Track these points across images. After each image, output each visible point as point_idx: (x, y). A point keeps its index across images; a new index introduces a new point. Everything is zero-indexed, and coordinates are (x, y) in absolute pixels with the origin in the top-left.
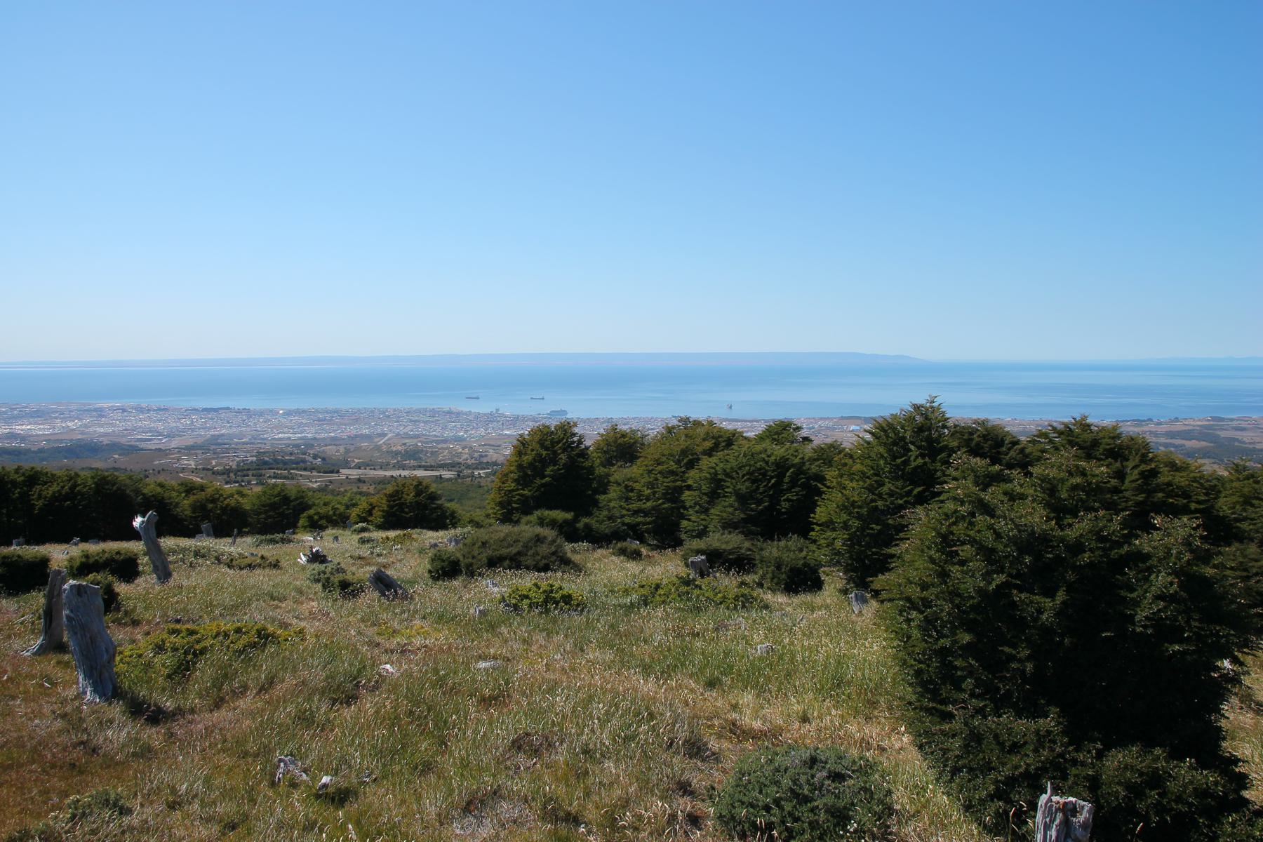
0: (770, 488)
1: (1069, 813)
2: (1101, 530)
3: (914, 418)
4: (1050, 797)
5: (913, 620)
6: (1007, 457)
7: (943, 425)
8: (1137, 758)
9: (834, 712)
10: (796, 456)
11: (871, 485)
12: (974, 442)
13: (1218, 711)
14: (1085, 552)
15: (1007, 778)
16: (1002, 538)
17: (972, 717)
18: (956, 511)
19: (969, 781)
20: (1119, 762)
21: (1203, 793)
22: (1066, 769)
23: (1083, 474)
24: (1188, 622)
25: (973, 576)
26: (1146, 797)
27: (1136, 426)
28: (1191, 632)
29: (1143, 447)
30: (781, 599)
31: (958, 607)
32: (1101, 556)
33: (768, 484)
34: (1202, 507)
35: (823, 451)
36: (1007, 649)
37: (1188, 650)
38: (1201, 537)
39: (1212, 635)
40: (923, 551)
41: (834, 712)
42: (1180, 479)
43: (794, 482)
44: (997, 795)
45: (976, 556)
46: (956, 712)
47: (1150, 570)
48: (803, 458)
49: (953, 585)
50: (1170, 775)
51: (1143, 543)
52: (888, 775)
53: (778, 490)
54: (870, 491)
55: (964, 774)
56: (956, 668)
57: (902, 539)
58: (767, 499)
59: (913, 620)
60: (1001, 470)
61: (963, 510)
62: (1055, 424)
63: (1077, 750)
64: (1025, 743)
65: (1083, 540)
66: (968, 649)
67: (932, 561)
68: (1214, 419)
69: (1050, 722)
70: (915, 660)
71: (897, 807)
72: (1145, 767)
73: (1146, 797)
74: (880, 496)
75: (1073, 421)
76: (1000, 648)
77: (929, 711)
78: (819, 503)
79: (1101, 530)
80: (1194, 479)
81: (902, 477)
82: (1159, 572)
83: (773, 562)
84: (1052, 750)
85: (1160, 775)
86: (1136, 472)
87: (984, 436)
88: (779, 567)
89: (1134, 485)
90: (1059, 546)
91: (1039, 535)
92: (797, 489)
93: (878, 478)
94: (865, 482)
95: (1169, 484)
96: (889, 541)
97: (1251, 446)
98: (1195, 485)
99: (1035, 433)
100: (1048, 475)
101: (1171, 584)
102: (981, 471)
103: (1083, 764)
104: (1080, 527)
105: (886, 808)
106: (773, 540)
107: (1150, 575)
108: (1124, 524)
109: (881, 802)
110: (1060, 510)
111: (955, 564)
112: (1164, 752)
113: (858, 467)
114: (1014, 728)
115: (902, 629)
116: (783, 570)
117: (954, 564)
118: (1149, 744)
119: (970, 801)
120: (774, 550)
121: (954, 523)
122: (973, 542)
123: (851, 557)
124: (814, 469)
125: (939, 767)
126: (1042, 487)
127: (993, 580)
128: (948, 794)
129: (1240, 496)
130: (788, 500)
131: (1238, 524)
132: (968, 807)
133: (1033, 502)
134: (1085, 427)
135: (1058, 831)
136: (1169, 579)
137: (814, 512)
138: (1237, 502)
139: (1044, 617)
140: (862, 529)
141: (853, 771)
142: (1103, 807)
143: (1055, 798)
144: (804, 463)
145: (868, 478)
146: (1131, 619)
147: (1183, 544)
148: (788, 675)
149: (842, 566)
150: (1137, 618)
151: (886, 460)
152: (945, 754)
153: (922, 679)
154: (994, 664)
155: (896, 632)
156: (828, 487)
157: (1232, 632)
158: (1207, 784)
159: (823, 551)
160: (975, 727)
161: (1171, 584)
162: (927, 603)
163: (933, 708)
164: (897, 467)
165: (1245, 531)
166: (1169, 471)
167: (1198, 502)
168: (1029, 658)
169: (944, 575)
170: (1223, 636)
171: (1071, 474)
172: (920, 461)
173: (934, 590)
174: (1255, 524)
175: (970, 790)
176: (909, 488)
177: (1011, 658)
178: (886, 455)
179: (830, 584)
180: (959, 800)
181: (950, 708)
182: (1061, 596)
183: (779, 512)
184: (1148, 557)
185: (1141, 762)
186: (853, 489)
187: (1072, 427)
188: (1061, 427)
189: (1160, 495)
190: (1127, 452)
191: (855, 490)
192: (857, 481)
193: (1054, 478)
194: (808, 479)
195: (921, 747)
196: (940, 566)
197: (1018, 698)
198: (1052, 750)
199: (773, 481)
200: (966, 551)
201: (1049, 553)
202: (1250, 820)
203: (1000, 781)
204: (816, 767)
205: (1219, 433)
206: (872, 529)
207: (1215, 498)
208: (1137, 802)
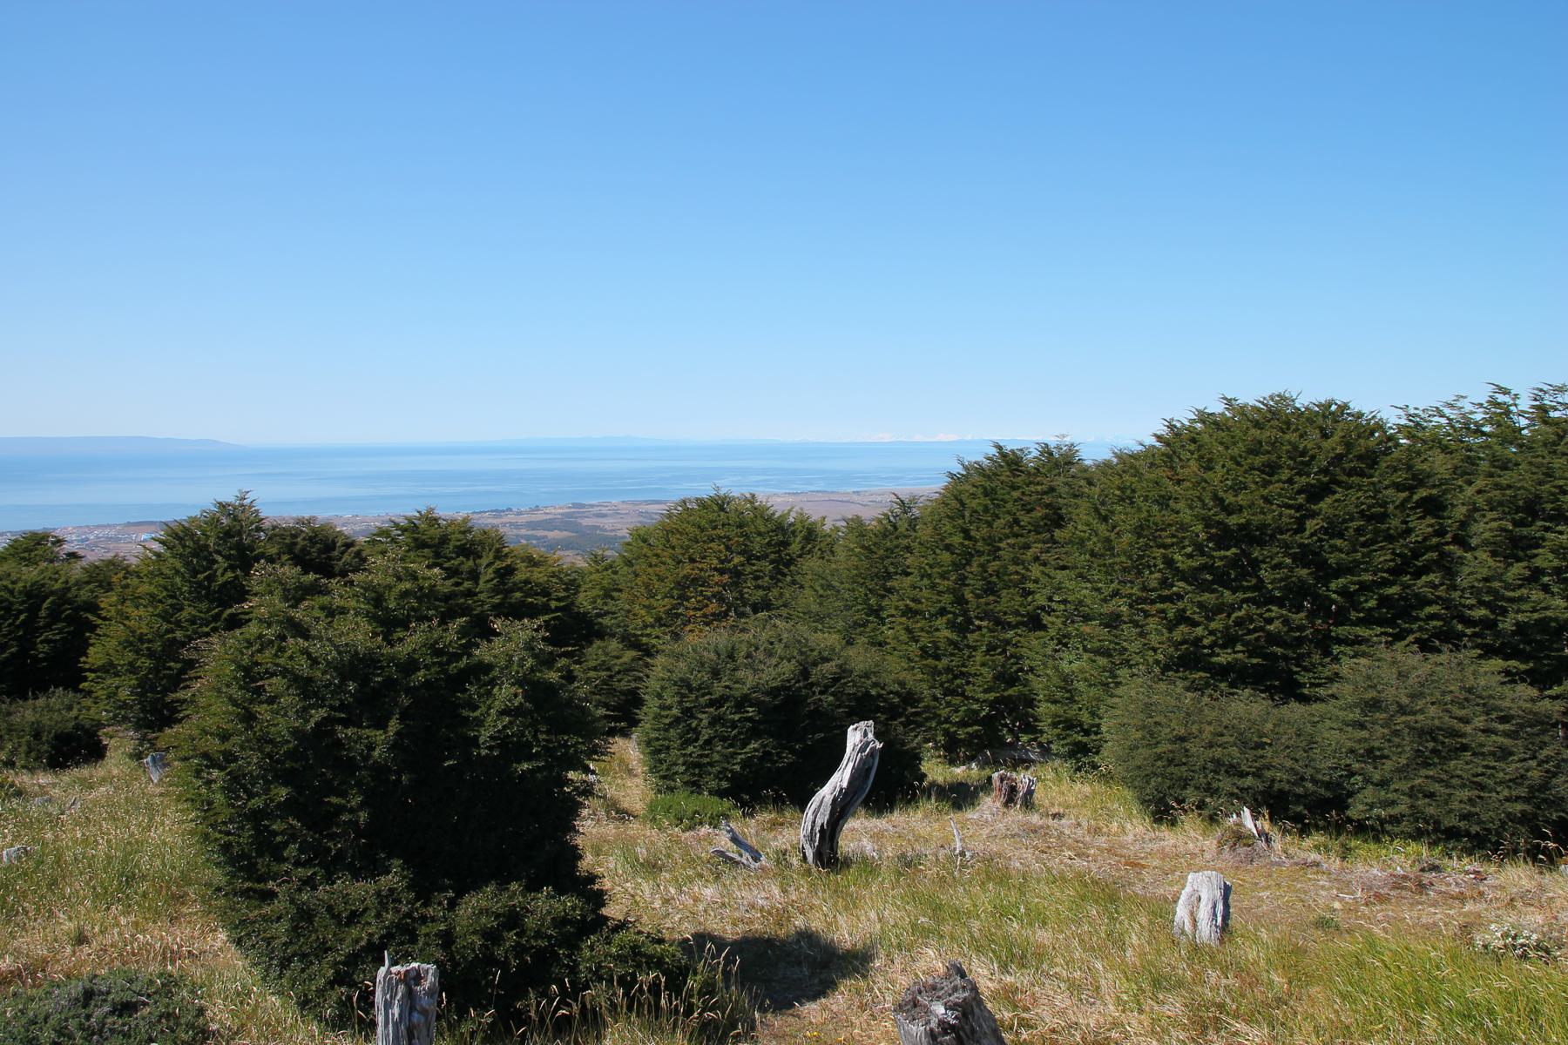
0: (18, 627)
1: (412, 982)
2: (436, 642)
3: (218, 521)
4: (389, 968)
5: (215, 781)
6: (341, 563)
7: (257, 527)
8: (492, 899)
9: (123, 921)
10: (56, 580)
11: (165, 611)
12: (298, 547)
13: (574, 830)
14: (419, 670)
15: (349, 956)
16: (319, 663)
17: (300, 890)
18: (260, 636)
19: (303, 970)
20: (473, 908)
21: (561, 922)
22: (415, 929)
23: (414, 576)
24: (535, 736)
25: (285, 715)
26: (504, 941)
27: (495, 517)
28: (538, 746)
29: (497, 541)
30: (44, 779)
31: (270, 756)
32: (437, 673)
33: (14, 622)
34: (562, 604)
35: (97, 571)
36: (335, 800)
37: (538, 767)
38: (544, 639)
39: (561, 746)
40: (219, 691)
41: (123, 921)
42: (539, 575)
43: (54, 615)
44: (340, 979)
45: (288, 689)
46: (277, 890)
47: (493, 682)
48: (67, 582)
49: (261, 730)
50: (528, 911)
51: (484, 652)
52: (201, 987)
53: (31, 628)
54: (164, 619)
55: (296, 964)
56: (275, 833)
57: (191, 679)
58: (14, 643)
59: (215, 781)
60: (316, 580)
61: (270, 633)
62: (397, 520)
63: (425, 905)
64: (366, 910)
65: (416, 656)
66: (288, 807)
67: (234, 702)
68: (575, 505)
69: (394, 878)
70: (220, 832)
71: (214, 1027)
72: (501, 907)
73: (504, 941)
74: (178, 623)
75: (418, 515)
76: (326, 800)
77: (246, 893)
78: (92, 641)
79: (436, 642)
80: (553, 575)
81: (207, 596)
82: (503, 683)
83: (27, 729)
84: (397, 911)
85: (518, 913)
86: (490, 570)
87: (311, 539)
88: (37, 735)
89: (489, 585)
90: (388, 666)
91: (365, 655)
92: (60, 625)
93: (175, 601)
94: (155, 608)
95: (527, 582)
96: (177, 682)
97: (613, 534)
98: (554, 580)
99: (375, 531)
100: (372, 581)
101: (516, 695)
102: (291, 583)
103: (433, 920)
104: (412, 641)
105: (197, 1034)
106: (26, 699)
107: (492, 688)
108: (463, 632)
109: (191, 1026)
110: (389, 624)
111: (263, 703)
112: (520, 886)
113: (145, 588)
114: (350, 894)
115: (200, 795)
116: (44, 739)
117: (261, 703)
118: (503, 884)
119: (306, 995)
120: (29, 712)
121: (259, 651)
122: (285, 672)
123: (143, 710)
124: (84, 595)
125: (265, 962)
126: (365, 598)
127: (311, 716)
128: (280, 993)
129: (601, 589)
130: (47, 641)
131: (600, 620)
132: (304, 1003)
133: (356, 615)
134: (432, 521)
135: (401, 1007)
136: (513, 690)
137: (86, 655)
138: (599, 596)
139: (376, 753)
140: (155, 670)
141: (149, 996)
142: (459, 964)
143: (394, 969)
144: (69, 589)
145: (160, 601)
146: (474, 742)
147: (525, 649)
148: (53, 883)
149: (130, 722)
150: (481, 740)
151: (183, 577)
152: (269, 944)
153: (232, 854)
154: (319, 818)
155: (192, 800)
156: (105, 619)
157: (580, 740)
158: (565, 911)
159: (101, 705)
160: (304, 903)
161: (516, 695)
162: (230, 757)
163: (249, 889)
164: (200, 584)
165: (608, 627)
166: (527, 567)
167: (558, 600)
168: (362, 806)
169: (249, 718)
170: (572, 746)
171: (400, 579)
172: (230, 574)
173: (235, 739)
174: (616, 618)
175: (304, 982)
176: (216, 610)
177: (340, 809)
178: (182, 570)
179: (117, 748)
180: (291, 998)
181: (271, 884)
182: (394, 725)
183: (35, 659)
184: (488, 668)
185: (497, 902)
186: (140, 617)
187: (416, 522)
188: (403, 523)
189: (518, 595)
190: (479, 548)
191: (142, 619)
192: (145, 606)
193: (379, 585)
194: (77, 609)
195: (239, 942)
196: (244, 708)
197: (353, 857)
198: (397, 911)
199: (22, 617)
200: (276, 684)
201: (379, 675)
202: (607, 937)
203: (339, 962)
204: (93, 1003)
205: (579, 520)
206: (170, 668)
207: (575, 594)
208: (495, 948)
